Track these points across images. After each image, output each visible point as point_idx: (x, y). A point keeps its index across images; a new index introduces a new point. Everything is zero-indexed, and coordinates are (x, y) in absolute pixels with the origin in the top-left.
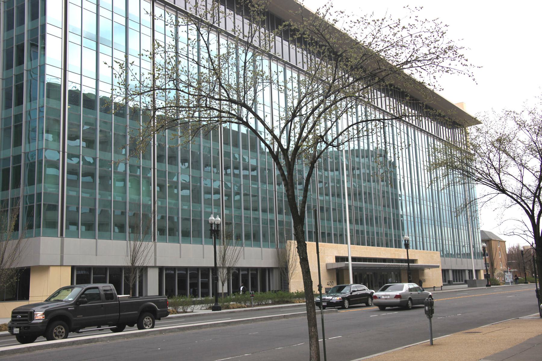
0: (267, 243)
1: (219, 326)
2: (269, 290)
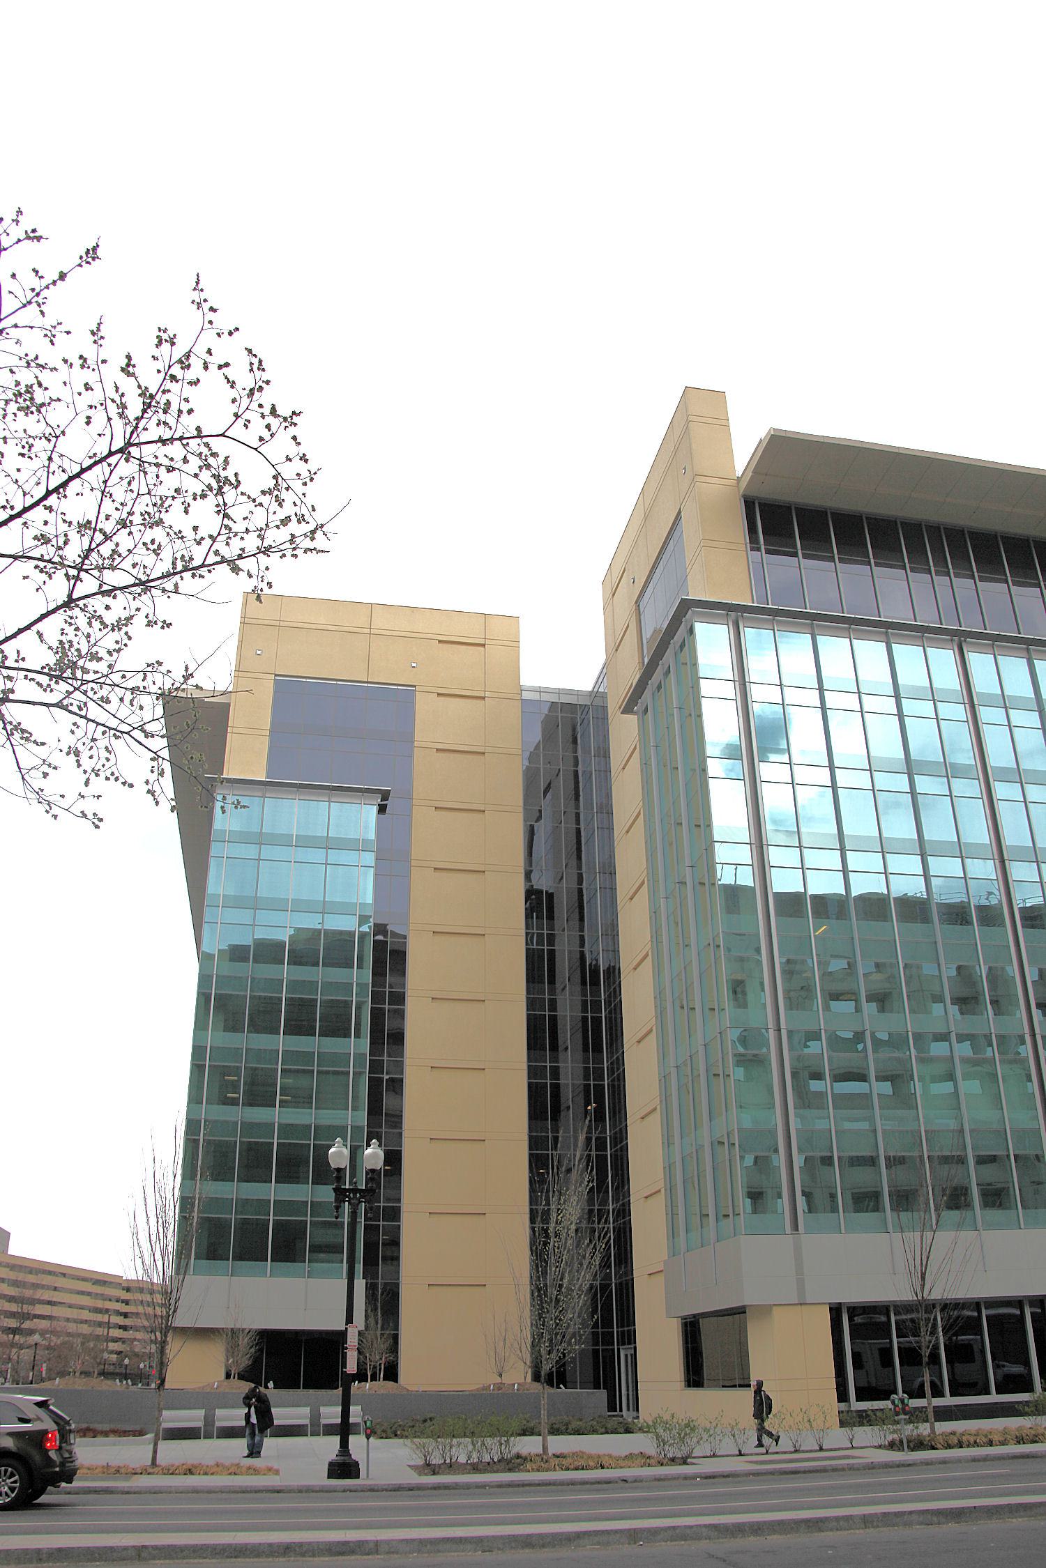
0: (239, 1197)
1: (908, 1524)
2: (609, 1416)
